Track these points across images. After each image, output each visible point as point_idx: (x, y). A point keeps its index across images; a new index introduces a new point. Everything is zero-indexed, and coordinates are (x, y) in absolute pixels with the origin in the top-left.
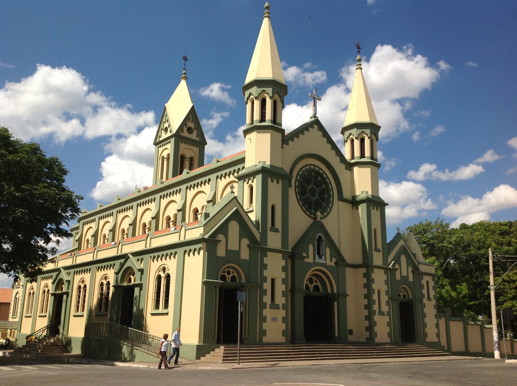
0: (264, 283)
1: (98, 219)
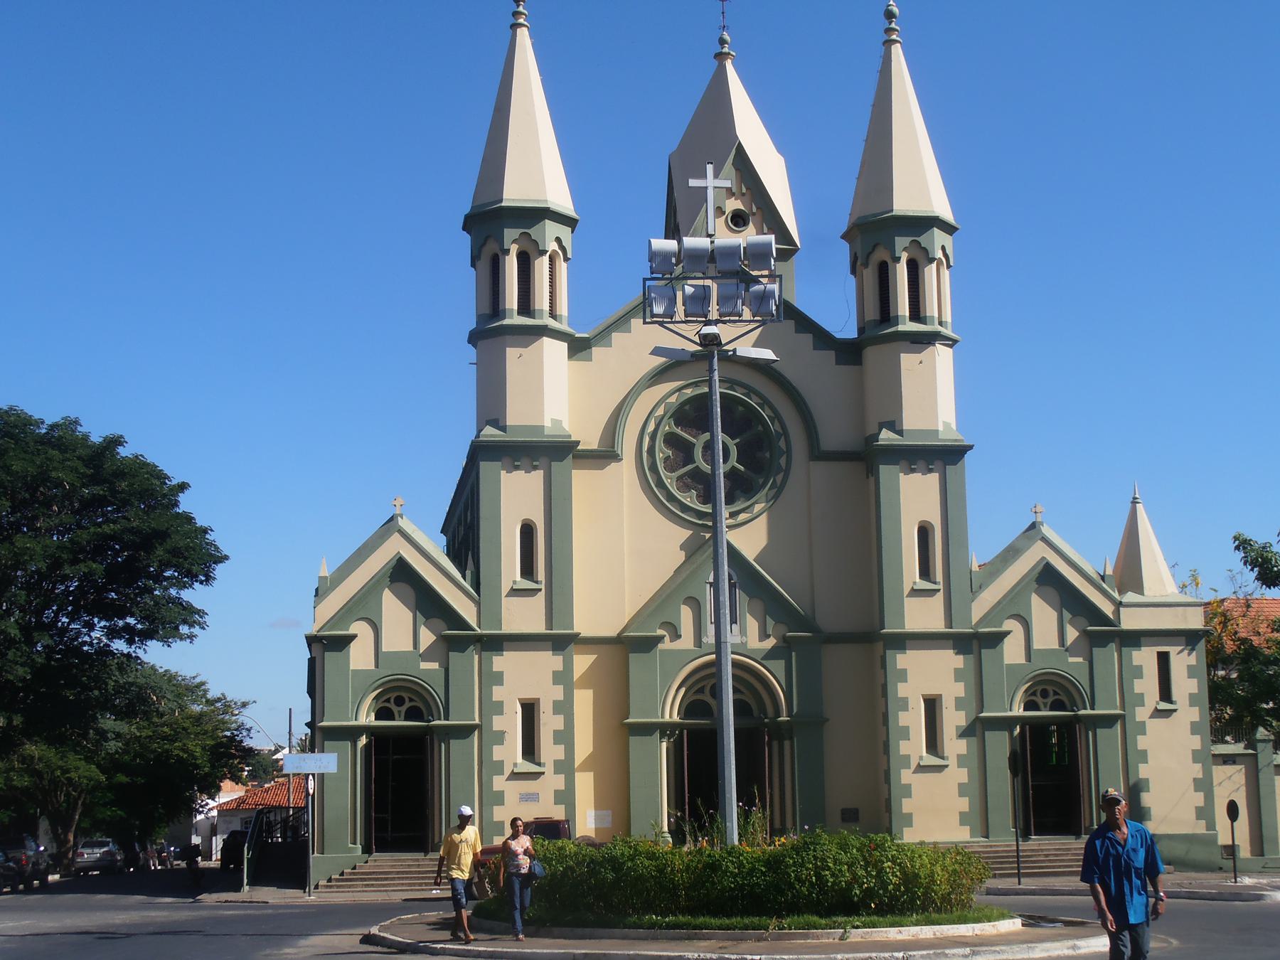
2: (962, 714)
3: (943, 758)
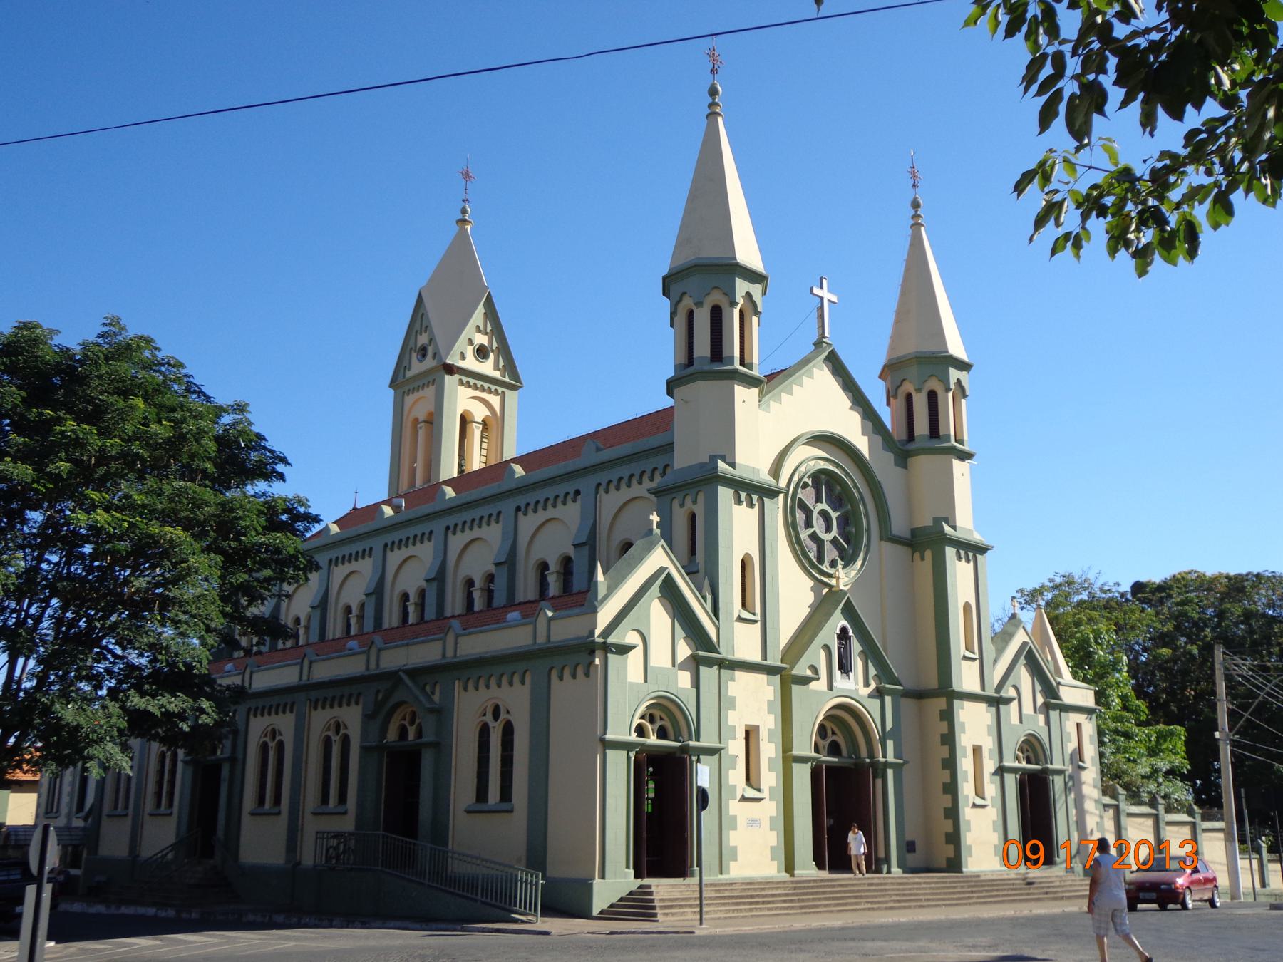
0: (730, 741)
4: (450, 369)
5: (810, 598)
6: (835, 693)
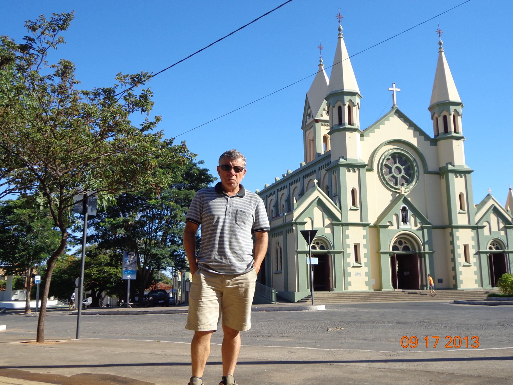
1: (302, 178)
2: (474, 250)
3: (470, 263)
4: (317, 121)
5: (391, 198)
6: (400, 230)
